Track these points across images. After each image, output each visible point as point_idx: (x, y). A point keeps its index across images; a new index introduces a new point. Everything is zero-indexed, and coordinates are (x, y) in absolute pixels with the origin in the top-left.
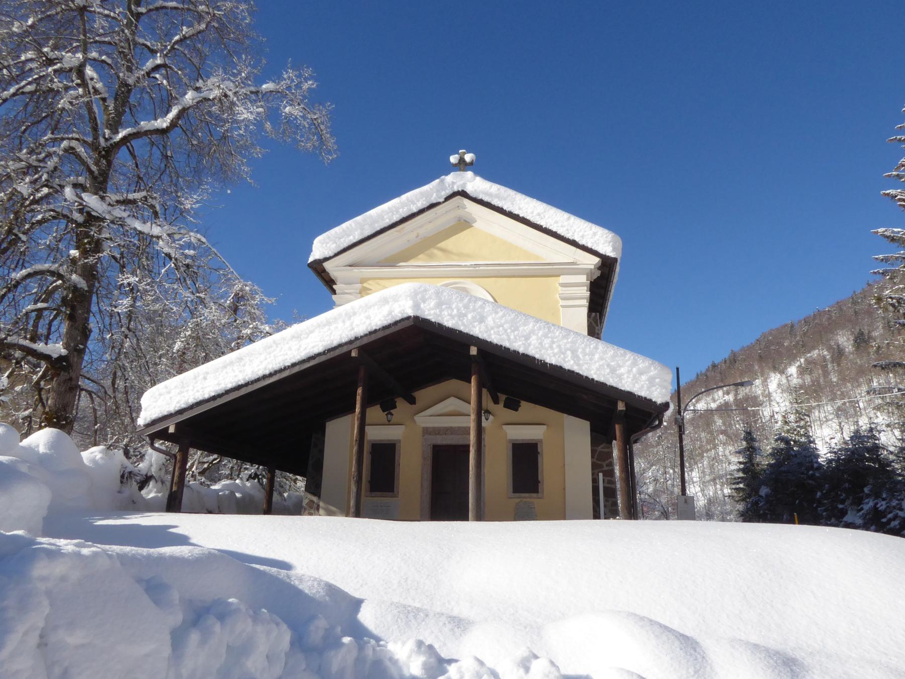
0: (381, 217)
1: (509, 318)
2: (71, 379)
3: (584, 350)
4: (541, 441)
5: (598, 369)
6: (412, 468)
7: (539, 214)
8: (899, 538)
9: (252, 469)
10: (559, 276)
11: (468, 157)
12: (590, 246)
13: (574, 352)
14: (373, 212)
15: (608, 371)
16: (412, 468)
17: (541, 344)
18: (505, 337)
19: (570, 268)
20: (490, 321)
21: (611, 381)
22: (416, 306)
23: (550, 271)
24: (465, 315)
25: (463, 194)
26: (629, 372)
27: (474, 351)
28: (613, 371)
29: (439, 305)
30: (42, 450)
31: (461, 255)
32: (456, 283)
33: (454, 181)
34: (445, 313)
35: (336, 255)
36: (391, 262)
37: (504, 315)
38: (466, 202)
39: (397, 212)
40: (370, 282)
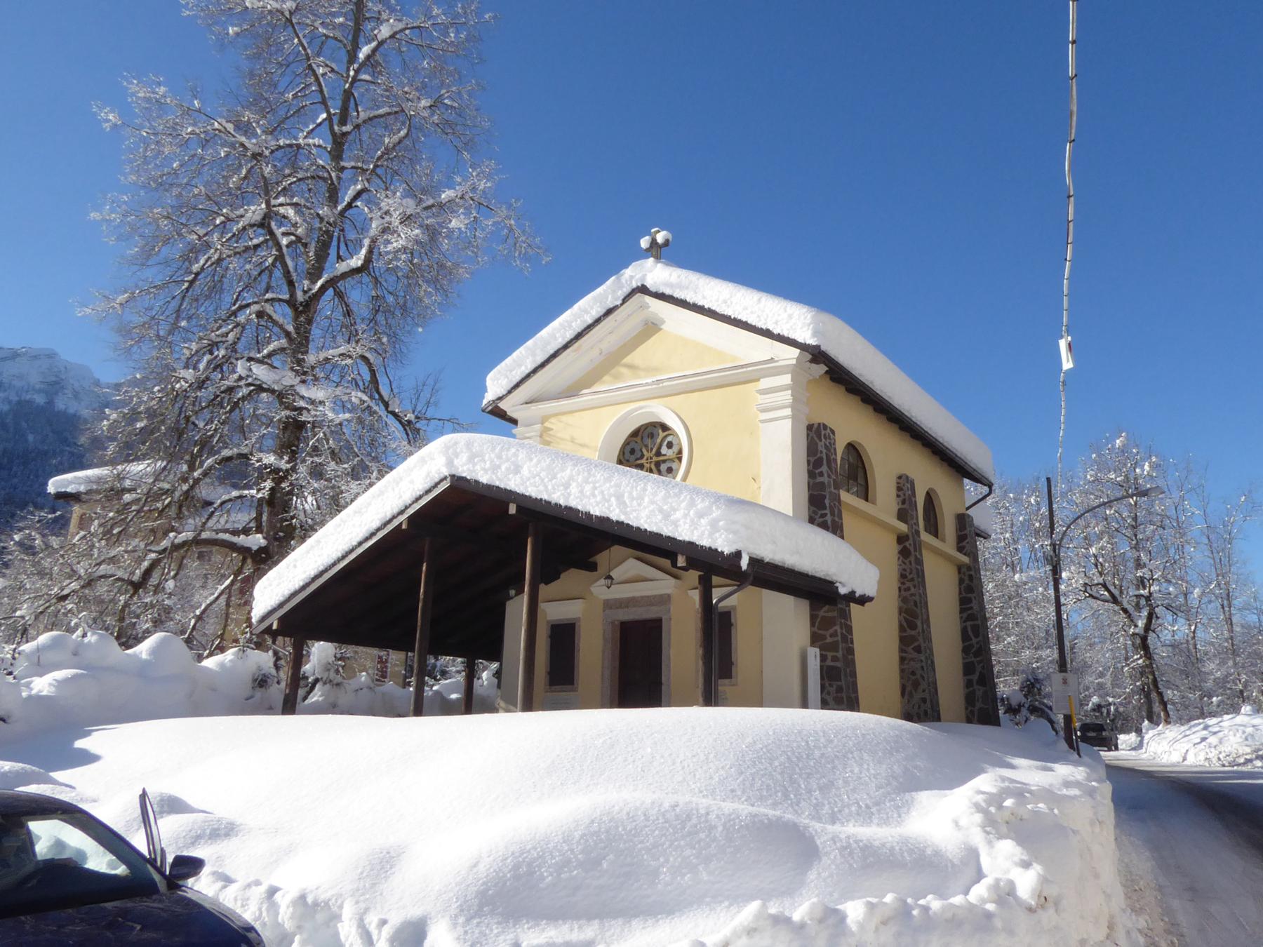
0: (553, 336)
1: (544, 464)
3: (630, 493)
5: (648, 517)
6: (593, 653)
7: (725, 302)
8: (486, 715)
9: (460, 660)
10: (758, 380)
11: (660, 238)
12: (786, 333)
13: (619, 497)
14: (544, 333)
15: (660, 517)
16: (593, 653)
17: (581, 492)
18: (541, 488)
19: (769, 368)
20: (525, 472)
21: (666, 531)
22: (450, 463)
23: (743, 376)
24: (499, 467)
25: (643, 290)
26: (686, 516)
27: (512, 509)
28: (666, 516)
29: (471, 459)
30: (144, 656)
31: (655, 370)
33: (634, 274)
34: (478, 467)
35: (510, 392)
36: (571, 391)
37: (539, 462)
38: (648, 299)
39: (570, 326)
40: (553, 420)
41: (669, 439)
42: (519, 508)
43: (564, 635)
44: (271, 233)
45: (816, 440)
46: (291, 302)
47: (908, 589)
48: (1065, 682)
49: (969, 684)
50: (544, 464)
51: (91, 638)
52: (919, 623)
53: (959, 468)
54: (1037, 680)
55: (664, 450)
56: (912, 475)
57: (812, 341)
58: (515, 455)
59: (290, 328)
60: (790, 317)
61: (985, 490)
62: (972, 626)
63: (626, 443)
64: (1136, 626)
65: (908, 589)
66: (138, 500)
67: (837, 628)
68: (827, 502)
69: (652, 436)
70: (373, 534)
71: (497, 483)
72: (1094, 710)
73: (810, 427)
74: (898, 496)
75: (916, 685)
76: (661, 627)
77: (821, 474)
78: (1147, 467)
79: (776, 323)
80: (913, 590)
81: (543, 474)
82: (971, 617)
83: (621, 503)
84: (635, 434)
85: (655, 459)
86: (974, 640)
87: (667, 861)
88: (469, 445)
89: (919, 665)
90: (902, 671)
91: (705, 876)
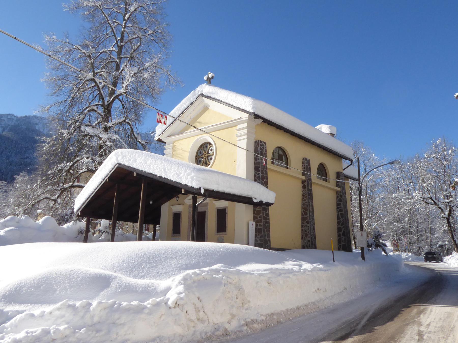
1: (143, 159)
4: (227, 207)
5: (173, 176)
10: (237, 126)
11: (210, 76)
12: (244, 108)
13: (164, 169)
15: (176, 176)
16: (186, 222)
17: (154, 168)
20: (138, 161)
22: (117, 159)
24: (130, 160)
25: (202, 95)
26: (184, 175)
27: (135, 175)
28: (178, 176)
30: (40, 224)
31: (206, 123)
32: (202, 137)
34: (124, 160)
38: (204, 98)
40: (176, 142)
41: (211, 148)
42: (137, 174)
43: (177, 217)
44: (95, 82)
45: (259, 148)
46: (103, 105)
47: (305, 200)
49: (339, 235)
50: (143, 159)
51: (23, 218)
52: (308, 213)
53: (339, 156)
54: (379, 235)
55: (210, 152)
56: (308, 158)
57: (252, 111)
58: (135, 156)
59: (102, 114)
60: (245, 102)
63: (199, 150)
64: (445, 214)
65: (305, 200)
66: (52, 173)
67: (262, 214)
68: (260, 169)
69: (206, 147)
70: (101, 183)
71: (130, 166)
72: (439, 247)
73: (256, 142)
75: (306, 235)
76: (205, 214)
78: (450, 151)
79: (241, 105)
80: (306, 201)
81: (143, 162)
82: (341, 211)
83: (165, 172)
84: (201, 146)
85: (207, 155)
86: (342, 219)
87: (60, 287)
88: (122, 153)
90: (302, 230)
91: (69, 292)
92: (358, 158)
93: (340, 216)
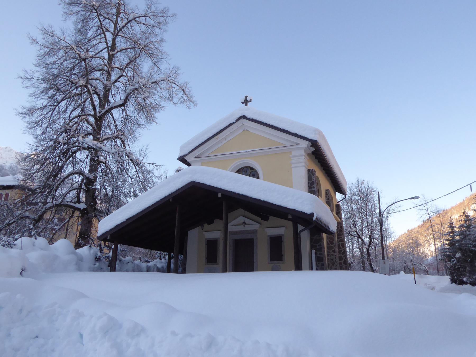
2: (88, 218)
4: (283, 235)
27: (220, 195)
42: (317, 218)
46: (95, 116)
48: (384, 263)
61: (344, 196)
62: (342, 244)
74: (326, 197)
77: (314, 187)
89: (334, 257)
92: (152, 83)
93: (341, 246)
